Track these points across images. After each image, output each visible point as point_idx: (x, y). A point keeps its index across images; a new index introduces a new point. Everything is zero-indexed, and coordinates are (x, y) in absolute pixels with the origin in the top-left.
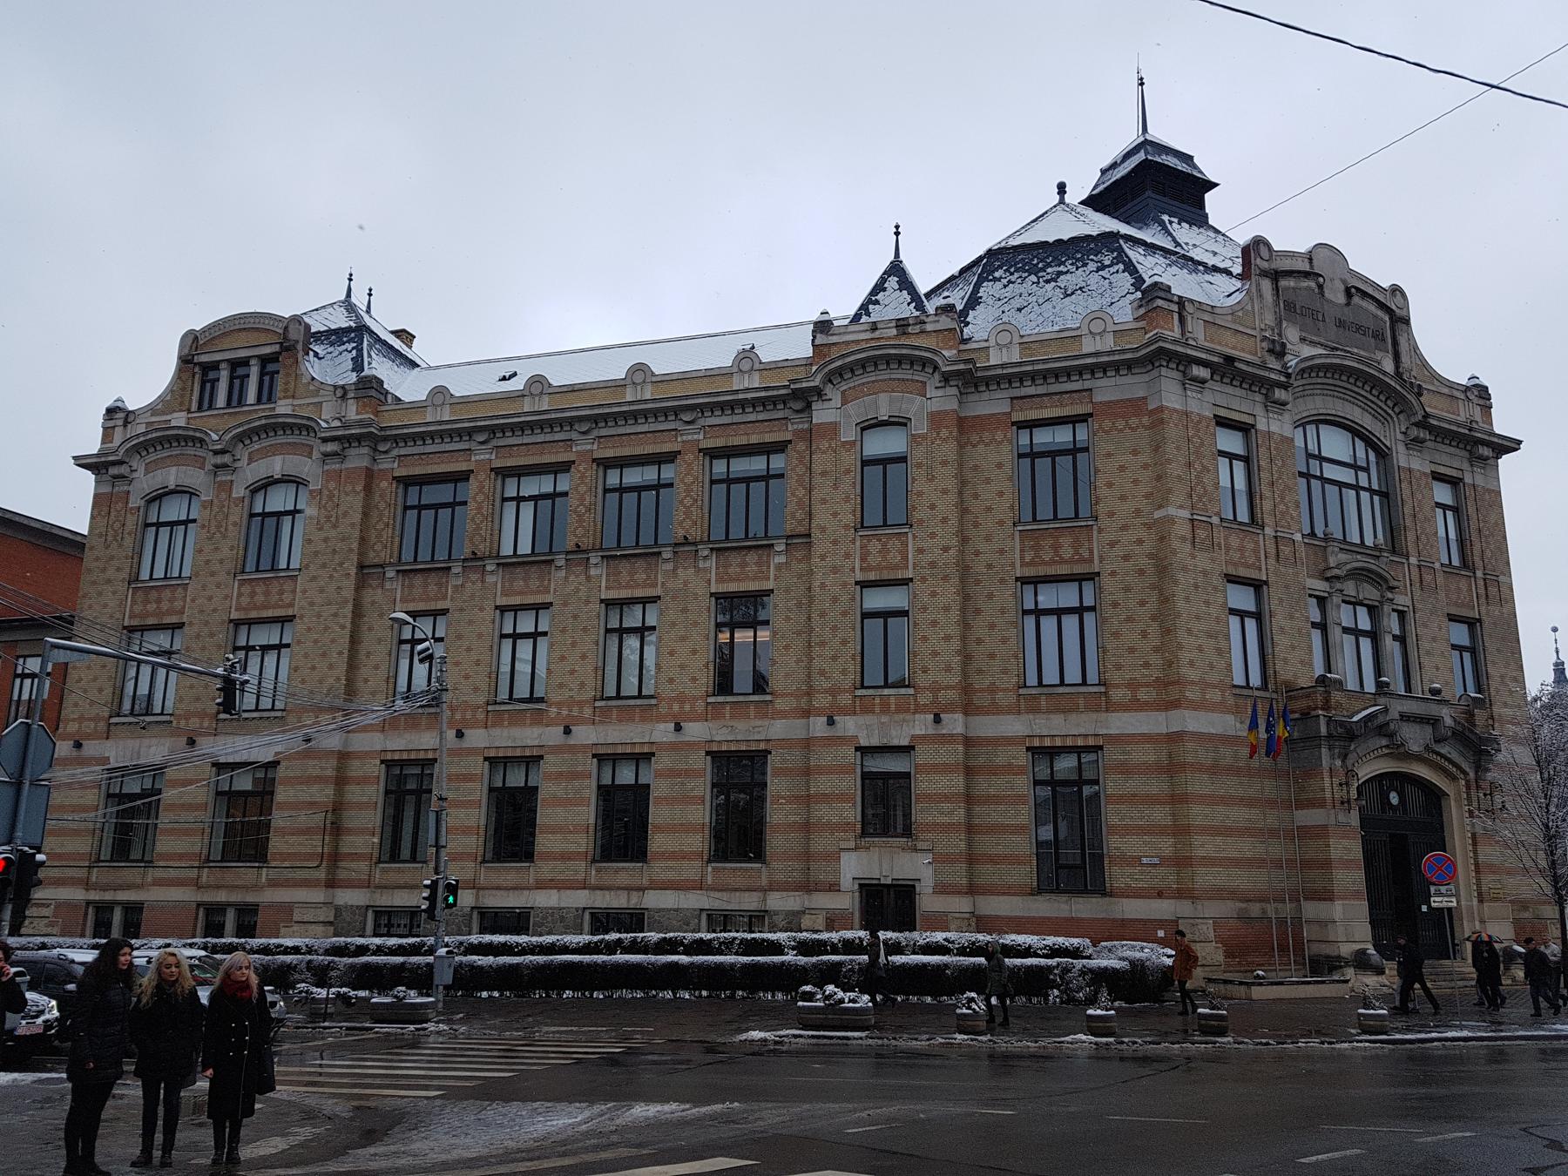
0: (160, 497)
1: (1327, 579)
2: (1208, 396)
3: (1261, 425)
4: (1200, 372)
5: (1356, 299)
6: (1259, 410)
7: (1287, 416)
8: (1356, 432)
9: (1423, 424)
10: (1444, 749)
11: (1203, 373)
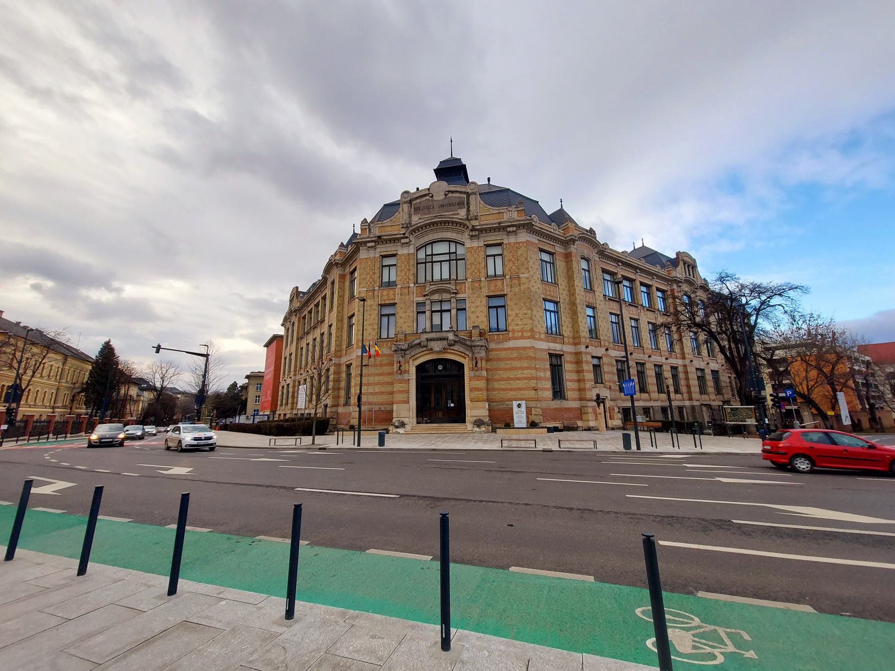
0: (432, 243)
1: (425, 296)
2: (378, 250)
3: (505, 242)
4: (512, 229)
5: (450, 195)
6: (505, 237)
7: (412, 247)
8: (449, 241)
9: (473, 229)
10: (455, 348)
11: (373, 244)
